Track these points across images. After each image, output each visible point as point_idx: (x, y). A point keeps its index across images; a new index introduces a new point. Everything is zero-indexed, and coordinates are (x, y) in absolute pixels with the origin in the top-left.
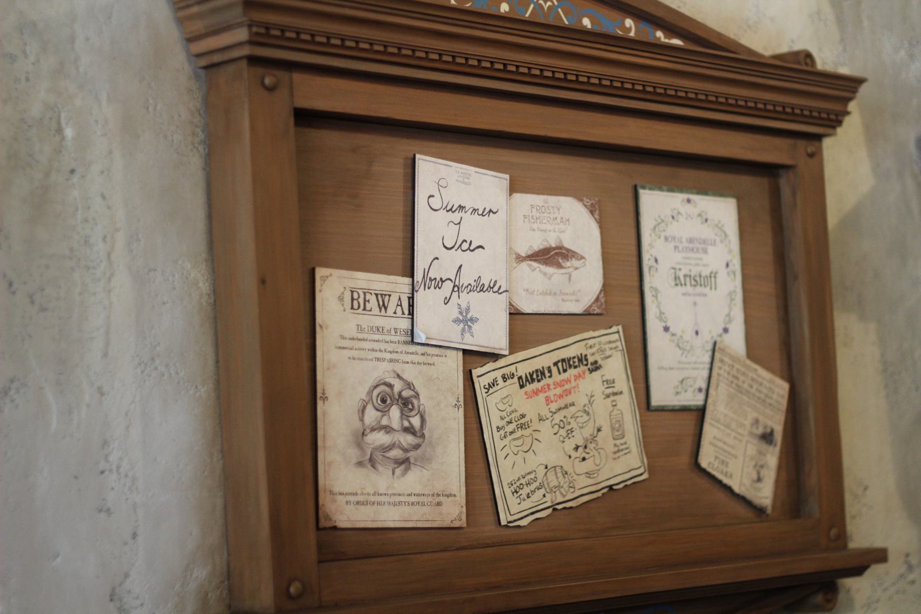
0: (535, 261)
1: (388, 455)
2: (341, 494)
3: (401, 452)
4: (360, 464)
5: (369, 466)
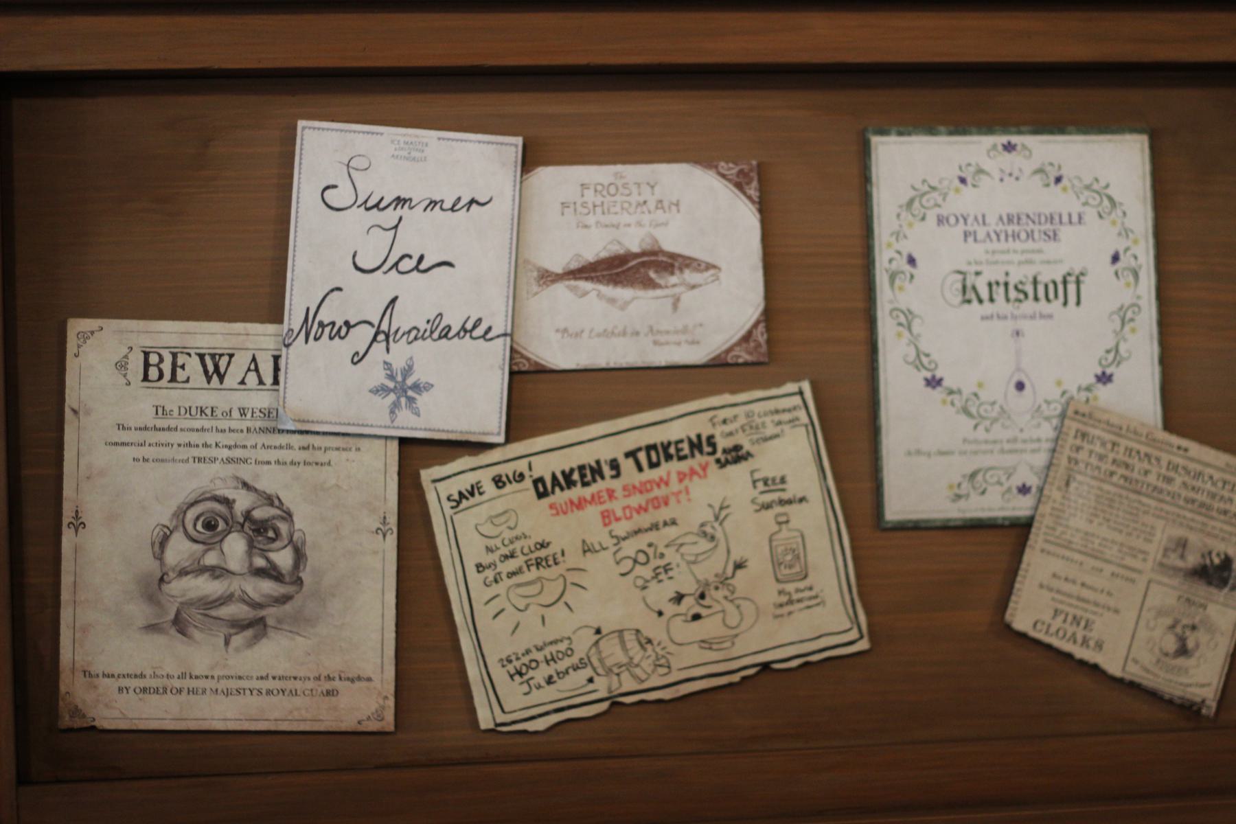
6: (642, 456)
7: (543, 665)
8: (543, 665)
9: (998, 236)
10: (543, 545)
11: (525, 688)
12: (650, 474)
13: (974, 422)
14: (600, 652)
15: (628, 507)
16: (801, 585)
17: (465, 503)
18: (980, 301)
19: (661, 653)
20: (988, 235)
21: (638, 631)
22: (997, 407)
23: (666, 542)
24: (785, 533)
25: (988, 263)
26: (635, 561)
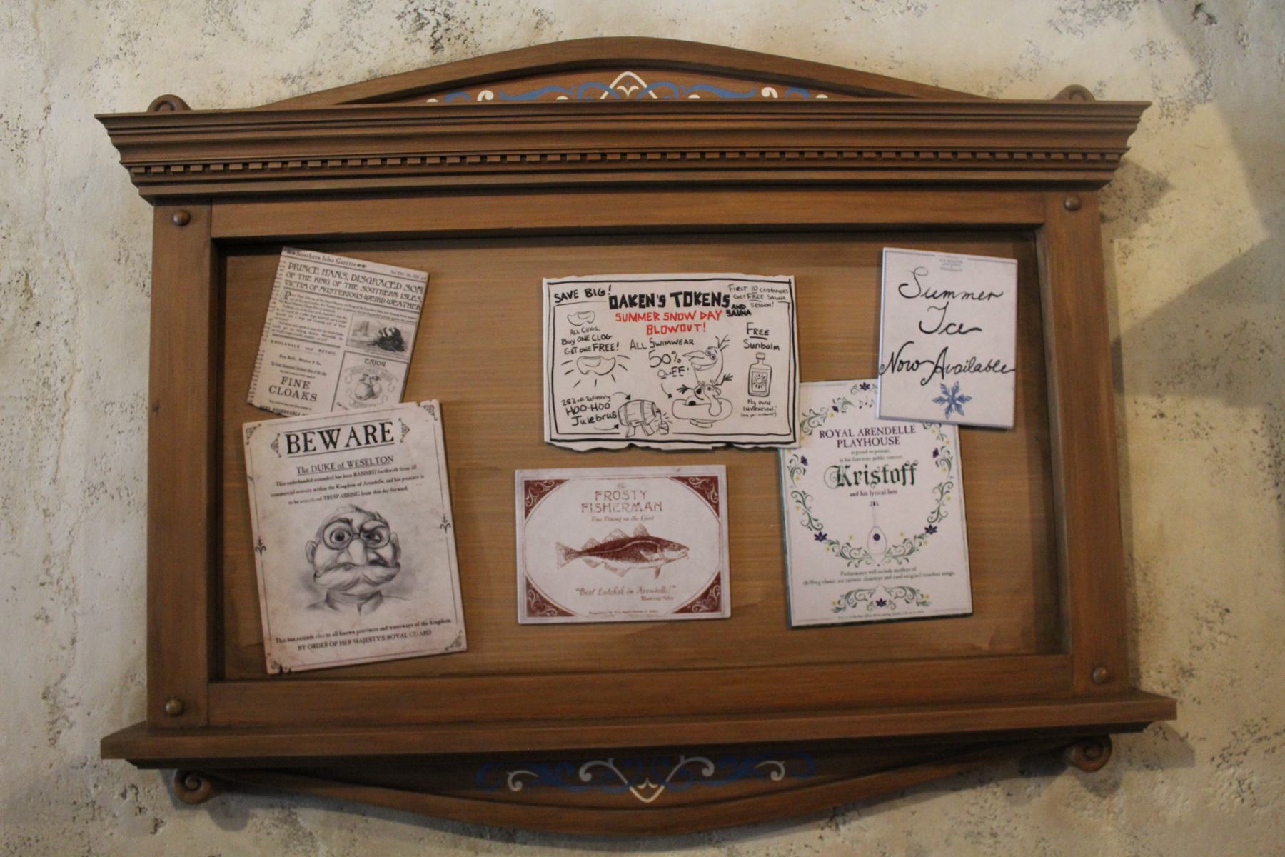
0: (598, 555)
1: (350, 592)
2: (290, 640)
3: (367, 586)
4: (313, 606)
5: (326, 607)
6: (681, 298)
7: (589, 410)
8: (589, 410)
9: (860, 443)
10: (607, 337)
11: (574, 421)
12: (683, 310)
13: (848, 561)
14: (626, 411)
15: (666, 326)
16: (763, 400)
17: (564, 301)
18: (850, 484)
19: (664, 420)
20: (853, 442)
21: (653, 403)
22: (862, 551)
23: (684, 353)
24: (760, 365)
25: (854, 460)
26: (662, 360)
